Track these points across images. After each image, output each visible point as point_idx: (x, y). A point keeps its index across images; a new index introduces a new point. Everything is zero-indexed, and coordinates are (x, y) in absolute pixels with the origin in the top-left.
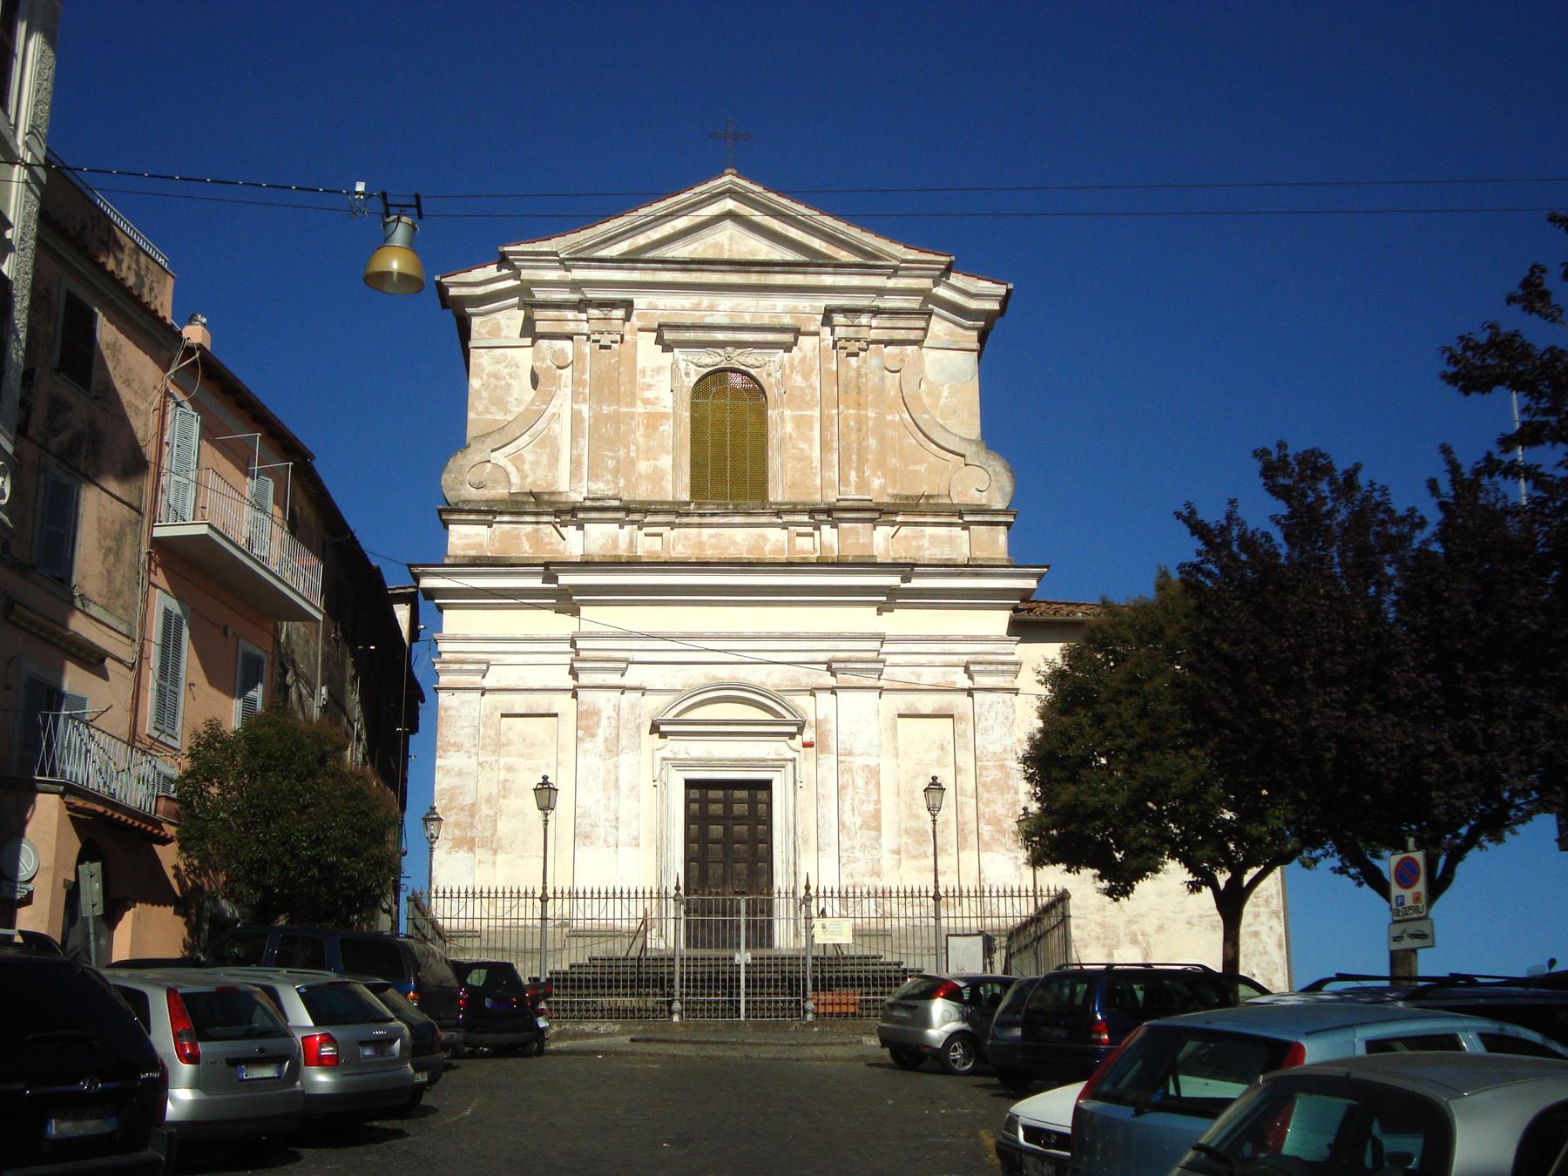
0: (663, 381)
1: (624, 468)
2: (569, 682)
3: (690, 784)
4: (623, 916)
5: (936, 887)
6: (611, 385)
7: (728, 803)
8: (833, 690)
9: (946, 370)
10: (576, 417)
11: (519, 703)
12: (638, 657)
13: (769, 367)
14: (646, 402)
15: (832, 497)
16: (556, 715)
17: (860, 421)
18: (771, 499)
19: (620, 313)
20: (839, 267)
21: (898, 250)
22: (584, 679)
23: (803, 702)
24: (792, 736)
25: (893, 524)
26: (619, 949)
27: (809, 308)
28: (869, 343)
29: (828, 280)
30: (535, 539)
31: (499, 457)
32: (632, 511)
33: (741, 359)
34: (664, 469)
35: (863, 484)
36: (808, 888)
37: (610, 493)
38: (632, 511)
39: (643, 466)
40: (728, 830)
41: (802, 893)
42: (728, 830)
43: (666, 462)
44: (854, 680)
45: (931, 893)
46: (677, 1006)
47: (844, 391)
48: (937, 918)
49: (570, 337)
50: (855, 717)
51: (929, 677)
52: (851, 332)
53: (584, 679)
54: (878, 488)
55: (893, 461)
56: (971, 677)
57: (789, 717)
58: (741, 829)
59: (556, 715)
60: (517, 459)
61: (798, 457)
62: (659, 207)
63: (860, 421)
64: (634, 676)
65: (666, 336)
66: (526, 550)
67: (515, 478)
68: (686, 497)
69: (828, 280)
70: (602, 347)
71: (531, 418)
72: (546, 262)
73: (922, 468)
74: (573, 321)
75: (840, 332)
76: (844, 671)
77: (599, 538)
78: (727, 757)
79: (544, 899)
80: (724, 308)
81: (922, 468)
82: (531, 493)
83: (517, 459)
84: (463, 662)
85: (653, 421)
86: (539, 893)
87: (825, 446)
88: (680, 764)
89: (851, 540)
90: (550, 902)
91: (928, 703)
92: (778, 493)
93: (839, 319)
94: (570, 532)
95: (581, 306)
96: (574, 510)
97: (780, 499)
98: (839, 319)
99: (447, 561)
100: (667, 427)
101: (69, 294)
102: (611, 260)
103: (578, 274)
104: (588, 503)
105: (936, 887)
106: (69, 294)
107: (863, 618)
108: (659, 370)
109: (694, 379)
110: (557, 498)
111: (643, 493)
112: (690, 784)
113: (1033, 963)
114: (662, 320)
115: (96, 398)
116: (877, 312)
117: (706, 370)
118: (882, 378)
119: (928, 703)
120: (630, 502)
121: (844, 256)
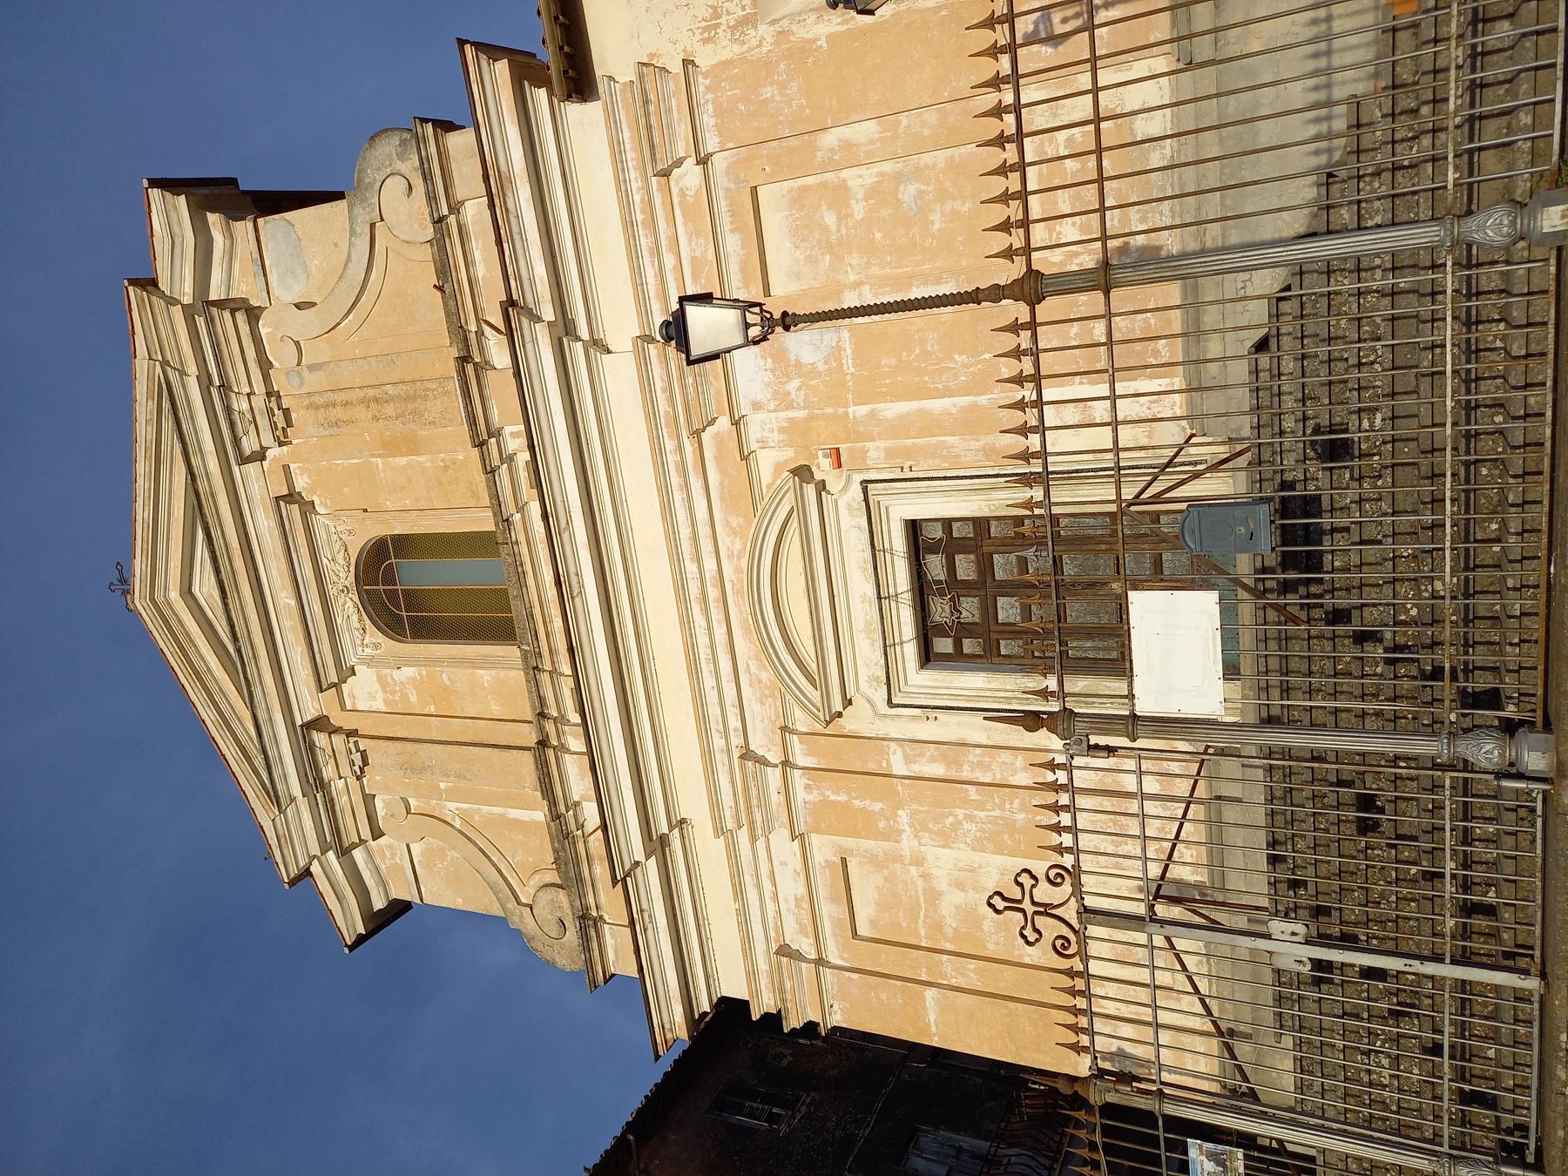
0: (384, 678)
3: (927, 657)
5: (996, 293)
7: (955, 587)
9: (293, 258)
13: (342, 540)
16: (844, 861)
19: (320, 738)
21: (141, 365)
24: (822, 487)
25: (480, 334)
33: (341, 574)
36: (1032, 721)
40: (1008, 588)
41: (1047, 740)
45: (1021, 311)
49: (369, 799)
52: (263, 422)
56: (679, 163)
58: (1003, 565)
59: (844, 861)
62: (196, 695)
65: (331, 680)
72: (294, 835)
75: (267, 439)
93: (249, 444)
99: (1166, 48)
105: (996, 293)
108: (382, 682)
109: (380, 638)
113: (1288, 233)
117: (368, 622)
118: (311, 368)
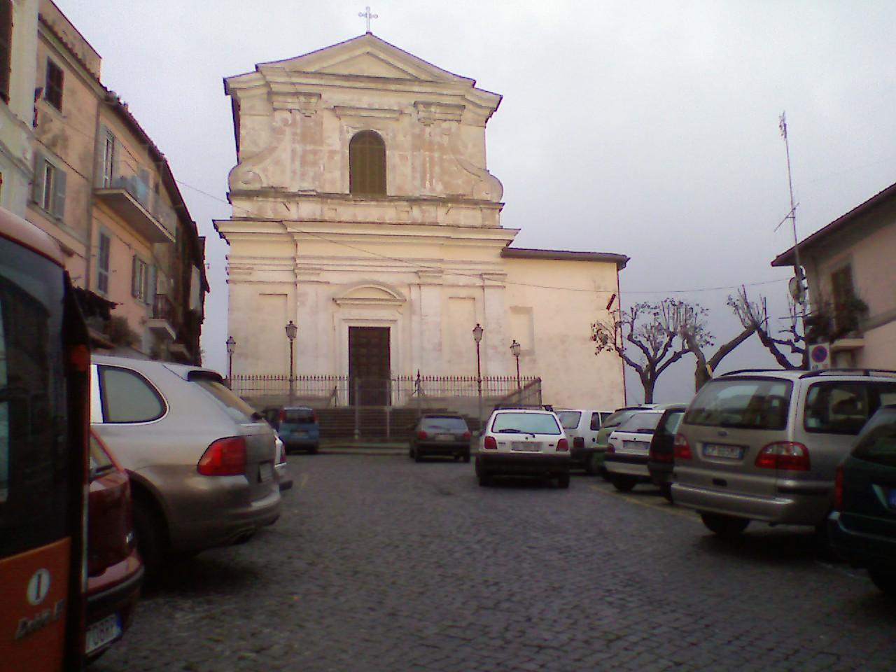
1: (317, 177)
2: (290, 278)
4: (320, 390)
6: (311, 136)
8: (419, 285)
10: (293, 151)
11: (268, 289)
12: (325, 268)
14: (329, 145)
15: (417, 194)
17: (432, 158)
18: (388, 194)
20: (421, 82)
22: (300, 278)
23: (404, 291)
26: (320, 406)
27: (405, 101)
28: (435, 120)
29: (416, 89)
30: (275, 211)
31: (257, 170)
32: (324, 197)
34: (337, 177)
35: (433, 190)
36: (419, 376)
37: (312, 188)
38: (324, 197)
39: (328, 176)
42: (369, 348)
43: (337, 174)
44: (429, 280)
46: (357, 431)
47: (420, 143)
48: (480, 391)
50: (430, 299)
51: (463, 281)
53: (300, 278)
54: (439, 190)
55: (446, 178)
57: (398, 298)
58: (363, 351)
60: (265, 170)
61: (401, 172)
63: (432, 158)
64: (324, 277)
65: (336, 110)
66: (270, 215)
67: (264, 179)
68: (348, 192)
69: (416, 89)
70: (306, 116)
71: (272, 150)
73: (460, 182)
74: (292, 103)
75: (422, 114)
76: (425, 275)
77: (307, 209)
78: (370, 317)
79: (480, 382)
80: (365, 100)
81: (460, 182)
82: (272, 187)
83: (265, 170)
84: (240, 268)
85: (332, 153)
86: (289, 377)
87: (414, 169)
88: (346, 320)
89: (427, 215)
90: (482, 383)
91: (463, 293)
92: (391, 191)
94: (293, 207)
95: (297, 94)
96: (294, 195)
97: (393, 194)
98: (421, 107)
100: (337, 158)
101: (48, 58)
102: (312, 73)
103: (294, 80)
104: (300, 193)
106: (48, 58)
107: (433, 252)
110: (285, 190)
111: (328, 189)
112: (350, 328)
114: (335, 105)
115: (65, 117)
116: (440, 105)
119: (463, 293)
120: (321, 193)
121: (423, 77)
